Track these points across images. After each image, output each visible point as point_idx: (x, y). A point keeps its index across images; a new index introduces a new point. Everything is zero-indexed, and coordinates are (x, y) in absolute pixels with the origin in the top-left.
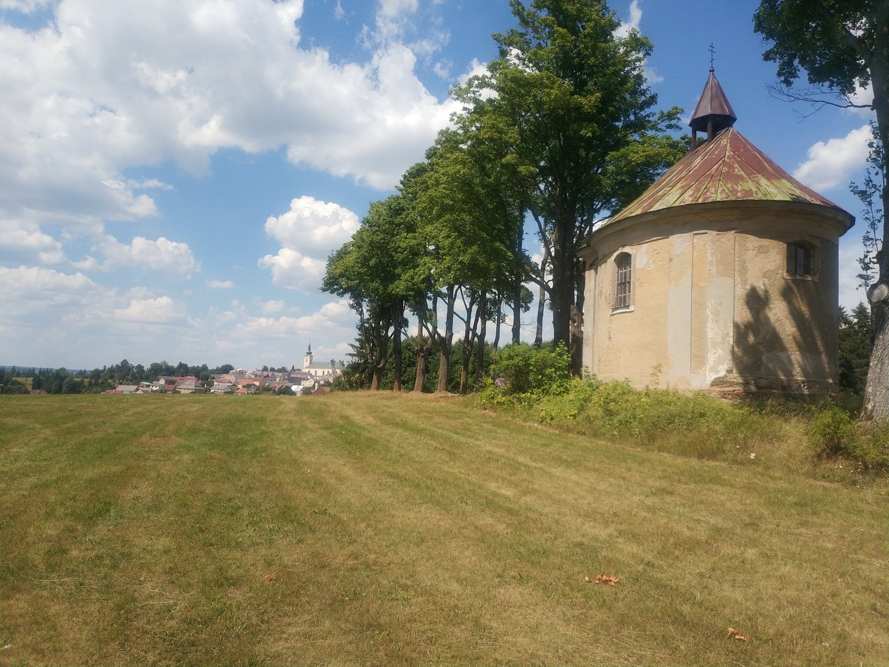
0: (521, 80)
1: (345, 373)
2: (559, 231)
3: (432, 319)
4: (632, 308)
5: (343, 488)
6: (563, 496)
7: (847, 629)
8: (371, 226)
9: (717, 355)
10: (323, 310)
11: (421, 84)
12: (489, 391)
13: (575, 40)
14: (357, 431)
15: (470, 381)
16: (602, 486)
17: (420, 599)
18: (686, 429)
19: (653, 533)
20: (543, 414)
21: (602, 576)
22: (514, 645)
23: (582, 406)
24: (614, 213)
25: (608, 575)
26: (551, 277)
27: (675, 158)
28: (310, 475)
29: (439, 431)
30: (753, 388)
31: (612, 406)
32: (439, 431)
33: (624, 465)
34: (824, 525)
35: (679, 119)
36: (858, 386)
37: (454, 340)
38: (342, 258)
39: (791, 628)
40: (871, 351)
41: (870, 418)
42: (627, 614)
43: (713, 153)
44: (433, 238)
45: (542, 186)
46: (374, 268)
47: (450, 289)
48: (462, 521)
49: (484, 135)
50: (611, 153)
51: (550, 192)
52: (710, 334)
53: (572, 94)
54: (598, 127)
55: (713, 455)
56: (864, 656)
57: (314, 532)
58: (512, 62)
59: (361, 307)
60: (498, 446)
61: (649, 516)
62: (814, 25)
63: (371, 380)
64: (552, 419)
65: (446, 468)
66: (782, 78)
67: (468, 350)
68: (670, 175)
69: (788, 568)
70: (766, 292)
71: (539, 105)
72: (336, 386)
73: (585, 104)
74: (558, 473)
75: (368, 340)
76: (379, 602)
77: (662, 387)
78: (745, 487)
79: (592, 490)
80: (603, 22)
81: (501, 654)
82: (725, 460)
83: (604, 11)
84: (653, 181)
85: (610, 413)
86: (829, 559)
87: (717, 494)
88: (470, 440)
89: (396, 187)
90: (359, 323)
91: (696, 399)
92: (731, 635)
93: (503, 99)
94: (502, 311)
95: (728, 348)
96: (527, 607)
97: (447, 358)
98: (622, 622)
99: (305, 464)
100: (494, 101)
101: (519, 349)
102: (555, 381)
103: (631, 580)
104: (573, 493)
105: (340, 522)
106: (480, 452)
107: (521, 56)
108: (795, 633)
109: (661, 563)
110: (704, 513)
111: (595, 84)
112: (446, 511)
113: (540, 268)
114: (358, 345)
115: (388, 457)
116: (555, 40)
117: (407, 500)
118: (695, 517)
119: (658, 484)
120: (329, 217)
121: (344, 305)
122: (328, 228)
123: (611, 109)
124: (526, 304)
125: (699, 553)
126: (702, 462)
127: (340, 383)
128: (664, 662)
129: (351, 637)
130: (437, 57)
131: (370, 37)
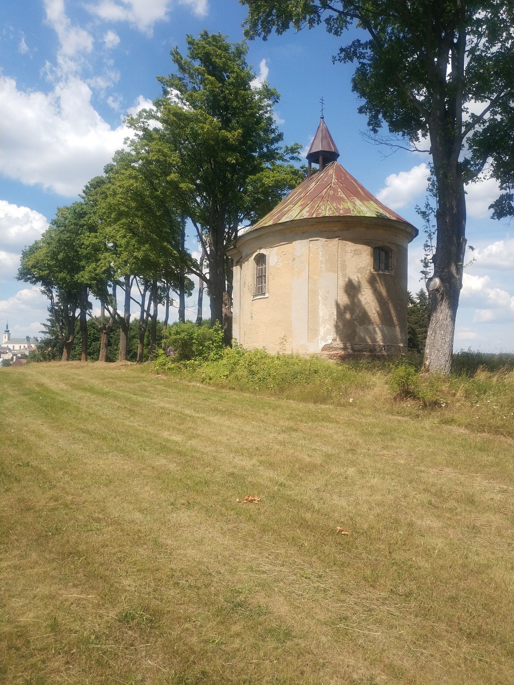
0: (181, 115)
1: (39, 348)
2: (213, 235)
3: (112, 303)
4: (267, 295)
5: (42, 443)
6: (219, 438)
7: (414, 520)
8: (58, 227)
9: (326, 329)
10: (18, 295)
11: (96, 113)
12: (161, 360)
13: (221, 86)
14: (51, 395)
15: (146, 351)
16: (247, 428)
17: (110, 528)
18: (305, 382)
19: (284, 461)
20: (204, 375)
21: (249, 497)
22: (185, 556)
23: (232, 368)
24: (253, 223)
25: (253, 496)
26: (207, 270)
27: (296, 183)
28: (13, 435)
29: (121, 393)
30: (350, 351)
31: (254, 368)
32: (121, 393)
33: (263, 411)
34: (399, 447)
35: (299, 153)
36: (420, 347)
37: (131, 320)
38: (34, 252)
39: (379, 522)
40: (428, 325)
41: (427, 371)
42: (267, 524)
43: (323, 180)
44: (112, 238)
45: (198, 199)
46: (61, 261)
47: (127, 278)
48: (142, 463)
49: (153, 157)
50: (250, 176)
51: (205, 205)
52: (321, 314)
53: (220, 129)
54: (240, 156)
55: (324, 400)
56: (424, 537)
57: (19, 481)
58: (173, 100)
59: (51, 292)
60: (169, 402)
61: (281, 448)
62: (392, 90)
63: (61, 353)
64: (210, 379)
65: (127, 423)
66: (371, 127)
67: (142, 327)
68: (292, 196)
69: (376, 480)
70: (359, 282)
71: (195, 135)
72: (32, 358)
73: (231, 137)
74: (215, 421)
75: (57, 320)
76: (77, 534)
77: (288, 352)
78: (346, 423)
79: (240, 431)
80: (243, 74)
81: (175, 564)
82: (332, 403)
83: (243, 65)
84: (281, 199)
85: (253, 373)
86: (402, 472)
87: (327, 429)
88: (147, 399)
89: (79, 195)
90: (49, 306)
91: (312, 360)
92: (339, 531)
93: (166, 129)
94: (170, 296)
95: (333, 322)
96: (194, 526)
97: (126, 334)
98: (264, 530)
99: (9, 425)
100: (159, 131)
101: (185, 327)
102: (212, 350)
103: (270, 498)
104: (227, 435)
105: (41, 471)
106: (155, 408)
107: (180, 96)
108: (380, 526)
109: (290, 483)
110: (319, 444)
111: (238, 122)
112: (129, 457)
113: (199, 263)
114: (50, 325)
115: (79, 417)
116: (206, 85)
117: (96, 450)
118: (313, 447)
119: (286, 424)
120: (21, 218)
121: (35, 291)
122: (20, 227)
123: (249, 142)
124: (189, 291)
125: (316, 473)
126: (317, 406)
127: (35, 356)
128: (294, 556)
129: (55, 565)
130: (109, 92)
131: (52, 72)
